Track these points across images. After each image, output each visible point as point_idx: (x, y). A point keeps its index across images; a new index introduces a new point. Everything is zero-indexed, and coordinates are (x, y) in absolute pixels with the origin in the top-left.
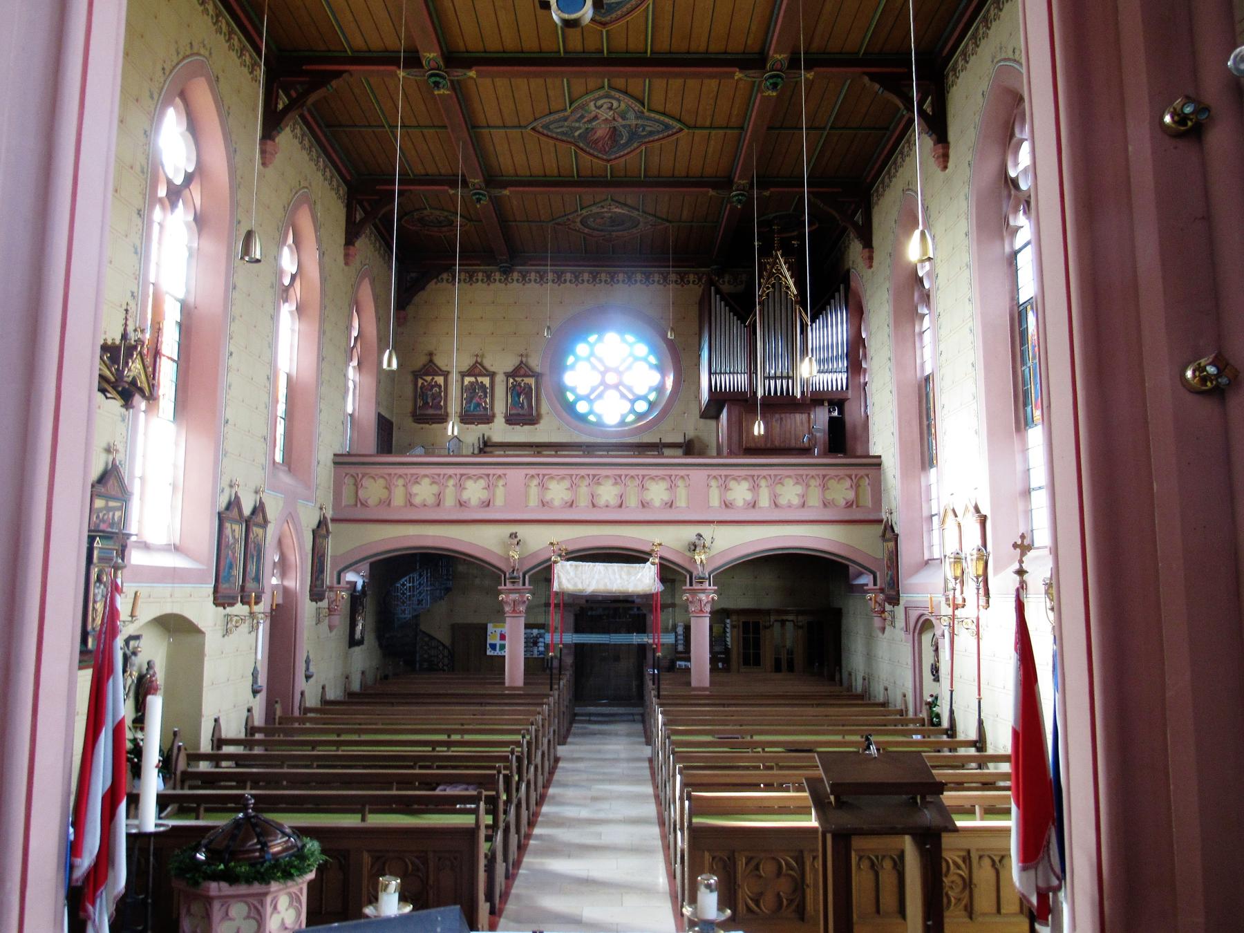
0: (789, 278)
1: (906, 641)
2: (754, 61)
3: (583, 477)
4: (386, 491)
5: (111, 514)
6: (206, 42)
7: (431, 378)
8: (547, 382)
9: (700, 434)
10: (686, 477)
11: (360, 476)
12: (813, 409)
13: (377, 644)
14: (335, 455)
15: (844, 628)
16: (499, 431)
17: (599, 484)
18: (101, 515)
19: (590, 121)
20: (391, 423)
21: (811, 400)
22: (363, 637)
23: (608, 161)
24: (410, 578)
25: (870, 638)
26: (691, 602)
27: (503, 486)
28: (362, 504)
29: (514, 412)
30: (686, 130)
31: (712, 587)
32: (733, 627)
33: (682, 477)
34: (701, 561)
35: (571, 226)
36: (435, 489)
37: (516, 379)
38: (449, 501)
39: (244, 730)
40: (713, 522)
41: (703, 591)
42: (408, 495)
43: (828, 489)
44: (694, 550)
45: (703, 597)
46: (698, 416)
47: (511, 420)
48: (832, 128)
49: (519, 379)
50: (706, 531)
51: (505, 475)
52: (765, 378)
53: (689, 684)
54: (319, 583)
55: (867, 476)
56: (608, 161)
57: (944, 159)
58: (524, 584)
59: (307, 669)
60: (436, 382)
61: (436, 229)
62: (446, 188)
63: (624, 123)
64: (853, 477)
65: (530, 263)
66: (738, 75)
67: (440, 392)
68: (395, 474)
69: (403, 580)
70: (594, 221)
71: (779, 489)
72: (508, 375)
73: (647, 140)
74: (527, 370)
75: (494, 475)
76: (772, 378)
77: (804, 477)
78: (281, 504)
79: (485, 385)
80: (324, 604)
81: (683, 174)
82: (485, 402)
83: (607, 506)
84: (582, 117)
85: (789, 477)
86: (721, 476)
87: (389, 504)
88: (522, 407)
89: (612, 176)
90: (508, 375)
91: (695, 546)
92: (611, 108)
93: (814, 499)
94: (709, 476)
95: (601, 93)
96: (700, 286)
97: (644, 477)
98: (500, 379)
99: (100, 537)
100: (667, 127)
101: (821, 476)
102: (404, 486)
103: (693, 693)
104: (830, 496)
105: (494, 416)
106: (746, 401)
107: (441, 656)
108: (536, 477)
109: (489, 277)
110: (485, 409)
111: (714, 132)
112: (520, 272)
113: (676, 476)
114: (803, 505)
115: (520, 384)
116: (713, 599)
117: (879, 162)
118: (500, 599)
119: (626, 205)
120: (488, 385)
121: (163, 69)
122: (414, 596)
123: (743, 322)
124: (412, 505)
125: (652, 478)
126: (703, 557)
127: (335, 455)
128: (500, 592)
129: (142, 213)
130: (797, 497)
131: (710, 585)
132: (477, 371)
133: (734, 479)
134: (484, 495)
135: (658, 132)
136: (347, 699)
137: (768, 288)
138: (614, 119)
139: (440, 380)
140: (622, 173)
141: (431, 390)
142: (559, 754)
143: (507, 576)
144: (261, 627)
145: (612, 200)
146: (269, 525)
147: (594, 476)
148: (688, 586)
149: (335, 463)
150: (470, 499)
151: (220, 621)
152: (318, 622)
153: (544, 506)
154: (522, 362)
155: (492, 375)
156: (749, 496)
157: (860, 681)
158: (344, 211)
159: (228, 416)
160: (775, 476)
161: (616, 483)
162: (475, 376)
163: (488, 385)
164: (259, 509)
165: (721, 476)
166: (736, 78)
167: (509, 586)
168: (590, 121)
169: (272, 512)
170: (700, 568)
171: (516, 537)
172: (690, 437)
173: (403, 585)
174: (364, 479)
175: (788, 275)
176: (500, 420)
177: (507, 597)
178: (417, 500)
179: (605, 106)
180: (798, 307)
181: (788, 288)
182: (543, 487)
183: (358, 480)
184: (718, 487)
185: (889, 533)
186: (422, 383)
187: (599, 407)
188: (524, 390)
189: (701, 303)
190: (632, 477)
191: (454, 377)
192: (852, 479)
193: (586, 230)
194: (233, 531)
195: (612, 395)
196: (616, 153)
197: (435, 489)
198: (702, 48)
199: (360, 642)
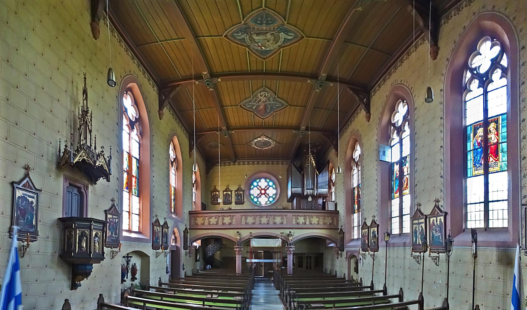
1: (346, 261)
2: (314, 76)
5: (114, 220)
6: (135, 72)
8: (247, 192)
14: (189, 211)
15: (324, 257)
16: (233, 206)
17: (262, 217)
18: (111, 220)
19: (258, 102)
20: (206, 205)
22: (199, 260)
23: (263, 119)
25: (333, 260)
29: (237, 201)
30: (288, 106)
32: (296, 258)
33: (285, 215)
38: (220, 223)
39: (168, 281)
40: (294, 228)
41: (291, 248)
47: (236, 203)
48: (332, 110)
49: (238, 192)
52: (306, 189)
54: (186, 245)
56: (263, 119)
57: (368, 118)
59: (183, 267)
61: (214, 149)
62: (216, 132)
63: (269, 103)
66: (309, 81)
71: (312, 219)
72: (235, 191)
73: (276, 110)
78: (173, 223)
80: (188, 251)
81: (286, 125)
84: (256, 100)
85: (315, 216)
88: (239, 200)
89: (264, 125)
90: (235, 191)
92: (265, 96)
93: (321, 222)
95: (262, 89)
99: (94, 221)
100: (283, 105)
103: (288, 276)
104: (325, 221)
105: (232, 202)
106: (301, 196)
109: (229, 164)
110: (230, 200)
111: (297, 107)
112: (238, 162)
114: (318, 224)
117: (353, 111)
120: (230, 194)
121: (121, 76)
123: (301, 173)
125: (277, 216)
126: (291, 238)
127: (189, 211)
129: (118, 124)
132: (227, 190)
133: (300, 216)
135: (280, 107)
138: (266, 101)
139: (218, 193)
140: (267, 125)
142: (253, 293)
144: (168, 255)
146: (169, 228)
147: (260, 215)
148: (287, 246)
151: (155, 254)
152: (186, 255)
155: (231, 191)
156: (304, 221)
157: (329, 271)
158: (189, 141)
159: (153, 195)
161: (266, 217)
163: (230, 194)
164: (166, 223)
166: (308, 82)
167: (237, 246)
168: (258, 102)
169: (170, 224)
170: (291, 241)
173: (210, 247)
176: (233, 203)
179: (263, 95)
181: (313, 164)
185: (342, 232)
189: (288, 170)
193: (256, 147)
194: (157, 229)
196: (266, 116)
197: (216, 220)
198: (297, 71)
199: (199, 261)
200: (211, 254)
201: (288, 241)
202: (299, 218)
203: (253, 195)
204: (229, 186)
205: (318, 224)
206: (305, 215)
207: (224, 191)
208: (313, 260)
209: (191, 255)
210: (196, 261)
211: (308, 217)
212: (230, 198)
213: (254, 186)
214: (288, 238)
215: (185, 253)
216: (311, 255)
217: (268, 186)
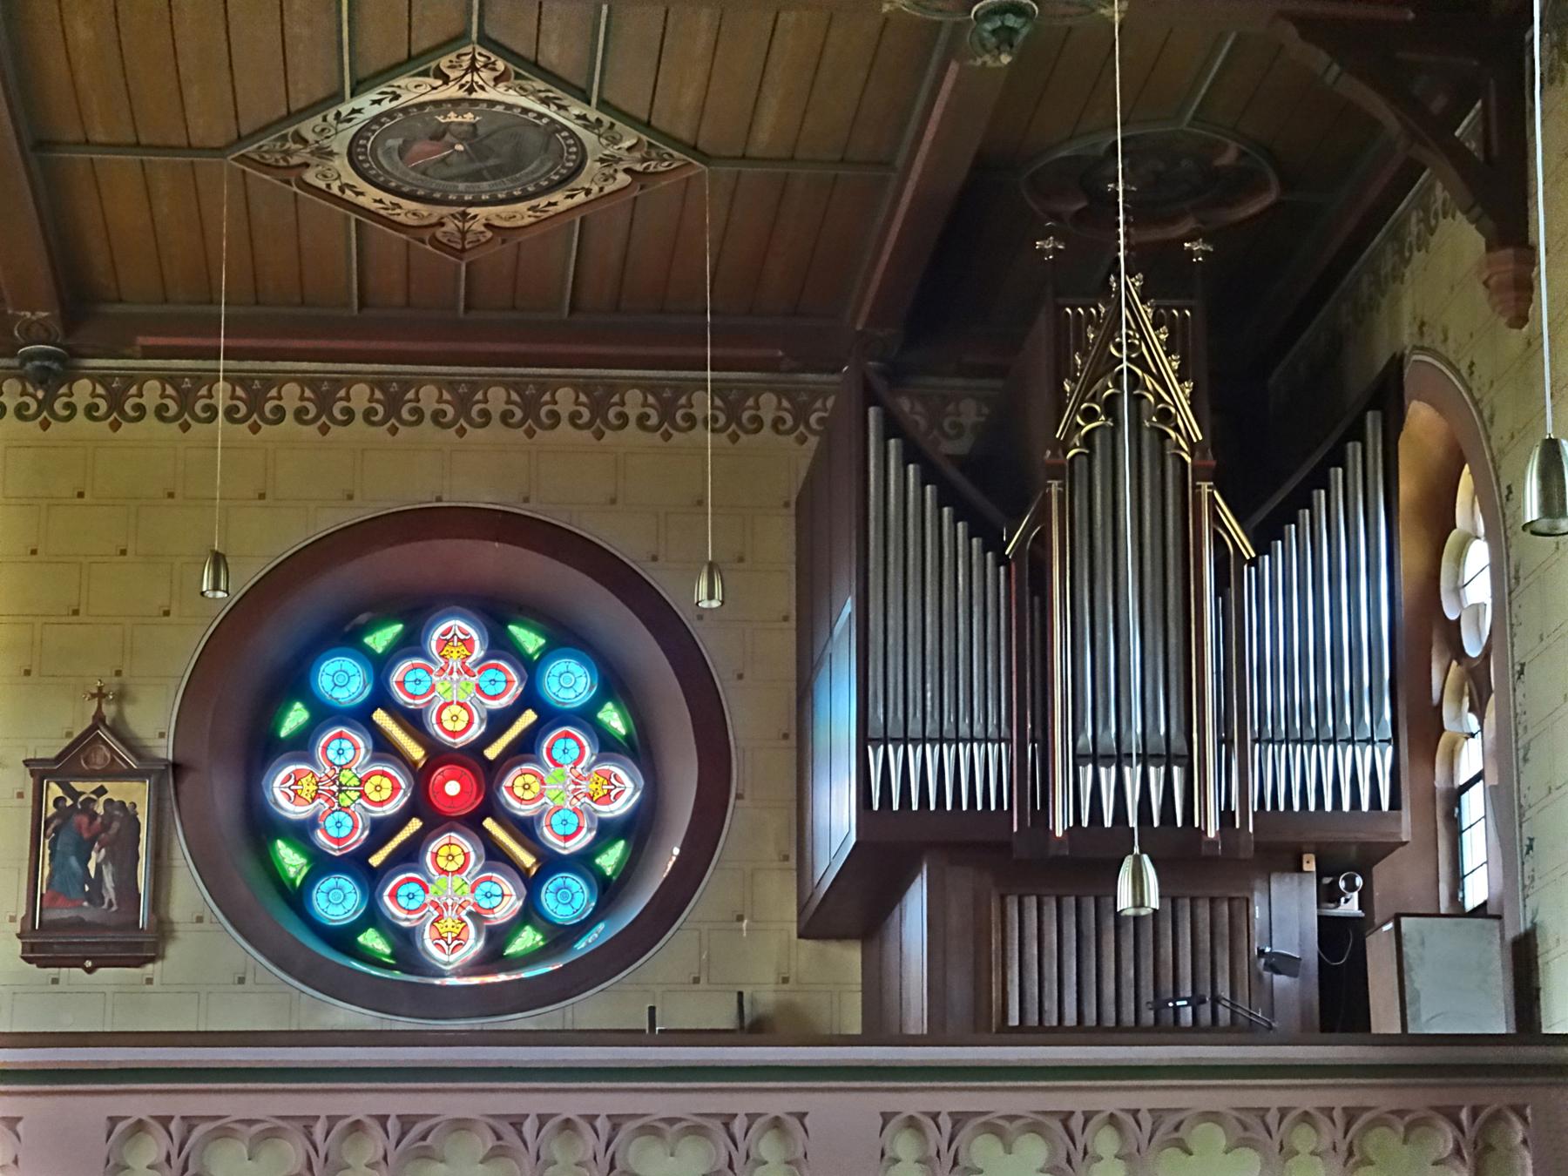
0: (1171, 378)
3: (357, 1126)
9: (798, 998)
10: (793, 1123)
12: (1259, 884)
21: (1258, 846)
35: (310, 176)
37: (78, 786)
46: (793, 929)
49: (85, 787)
52: (1079, 759)
55: (1519, 1111)
64: (1464, 1115)
65: (142, 340)
70: (402, 152)
76: (1107, 759)
77: (1272, 1118)
85: (1212, 1116)
86: (935, 1117)
88: (96, 896)
94: (886, 1117)
96: (802, 440)
97: (616, 1122)
101: (1337, 1114)
106: (1003, 847)
108: (157, 1128)
112: (101, 378)
113: (752, 1118)
119: (536, 68)
123: (994, 544)
125: (650, 1130)
137: (1090, 415)
145: (484, 40)
147: (407, 1122)
172: (761, 1010)
175: (1170, 366)
180: (1205, 487)
181: (1165, 416)
188: (106, 827)
190: (568, 1124)
192: (1458, 1125)
193: (370, 197)
203: (301, 833)
211: (1105, 1142)
213: (325, 715)
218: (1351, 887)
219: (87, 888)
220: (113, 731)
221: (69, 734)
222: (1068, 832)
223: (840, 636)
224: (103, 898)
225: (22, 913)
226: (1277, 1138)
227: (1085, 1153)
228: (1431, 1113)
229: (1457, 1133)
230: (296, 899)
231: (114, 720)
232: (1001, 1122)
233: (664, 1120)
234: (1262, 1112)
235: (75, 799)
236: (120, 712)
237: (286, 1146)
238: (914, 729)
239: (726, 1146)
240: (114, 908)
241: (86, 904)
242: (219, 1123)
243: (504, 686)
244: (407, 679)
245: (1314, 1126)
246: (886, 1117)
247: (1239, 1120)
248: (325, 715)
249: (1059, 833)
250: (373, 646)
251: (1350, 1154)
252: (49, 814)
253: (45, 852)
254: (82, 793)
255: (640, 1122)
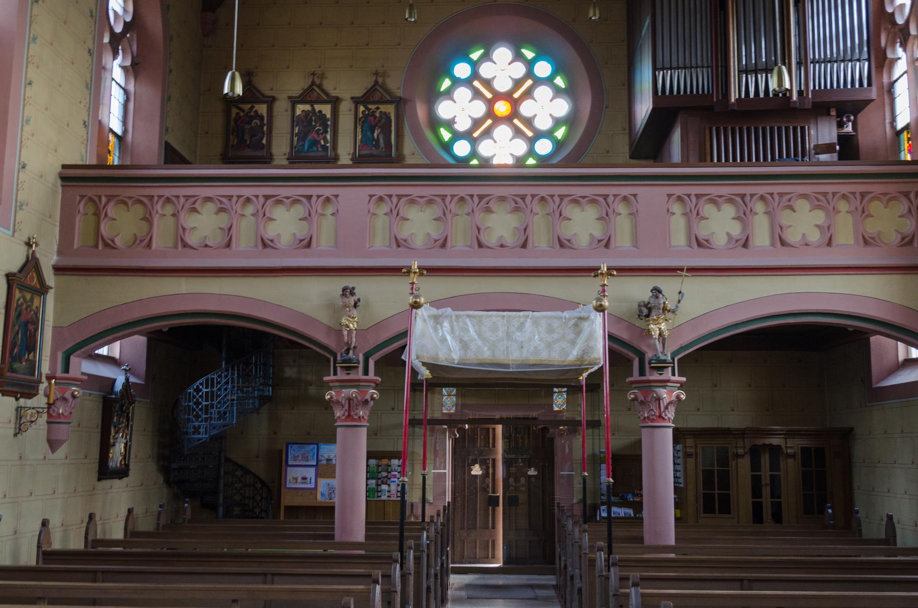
4: (144, 224)
7: (249, 106)
11: (104, 200)
13: (161, 479)
14: (64, 167)
17: (488, 210)
24: (207, 380)
26: (642, 403)
27: (332, 214)
28: (106, 245)
31: (677, 378)
33: (625, 199)
34: (660, 335)
36: (223, 220)
37: (370, 106)
41: (664, 383)
42: (181, 230)
43: (870, 216)
44: (648, 316)
45: (663, 393)
46: (628, 155)
50: (669, 286)
51: (336, 196)
53: (641, 540)
58: (366, 372)
60: (256, 112)
67: (262, 125)
68: (160, 197)
69: (198, 383)
71: (785, 217)
72: (357, 101)
74: (385, 94)
75: (319, 197)
77: (830, 196)
79: (325, 115)
82: (325, 139)
83: (502, 246)
85: (804, 196)
87: (149, 245)
88: (377, 146)
90: (357, 101)
91: (650, 310)
93: (845, 234)
98: (346, 108)
102: (173, 215)
104: (871, 227)
107: (258, 498)
110: (325, 148)
115: (373, 113)
116: (678, 397)
118: (327, 397)
120: (328, 116)
122: (212, 406)
124: (185, 245)
125: (575, 201)
128: (327, 386)
130: (817, 230)
131: (673, 374)
132: (314, 96)
133: (713, 201)
134: (301, 230)
136: (41, 565)
141: (250, 123)
143: (339, 358)
147: (481, 197)
148: (636, 376)
149: (64, 178)
150: (279, 235)
153: (399, 246)
154: (376, 82)
155: (335, 102)
156: (736, 229)
160: (781, 195)
161: (517, 209)
162: (311, 103)
163: (328, 116)
165: (689, 196)
167: (341, 375)
170: (659, 346)
171: (352, 294)
173: (198, 390)
174: (111, 204)
177: (338, 393)
178: (193, 239)
182: (395, 214)
183: (101, 207)
184: (684, 214)
186: (237, 114)
187: (485, 148)
188: (380, 121)
191: (281, 106)
195: (503, 132)
197: (223, 220)
199: (122, 473)
200: (203, 436)
201: (644, 348)
202: (708, 209)
203: (449, 124)
204: (323, 76)
205: (829, 244)
206: (743, 196)
207: (294, 101)
208: (790, 469)
209: (62, 431)
210: (105, 472)
211: (759, 207)
212: (328, 137)
213: (457, 82)
214: (639, 323)
215: (12, 415)
216: (775, 441)
217: (529, 82)
218: (849, 121)
219: (374, 143)
220: (381, 86)
221: (366, 88)
222: (736, 100)
223: (645, 35)
224: (379, 146)
225: (352, 151)
226: (832, 205)
227: (751, 211)
228: (898, 194)
229: (909, 203)
230: (447, 147)
231: (382, 83)
232: (716, 198)
233: (581, 197)
234: (825, 194)
235: (369, 111)
236: (384, 81)
237: (435, 207)
238: (674, 64)
239: (605, 207)
240: (384, 150)
241: (374, 148)
242: (410, 197)
243: (519, 70)
244: (486, 70)
245: (848, 201)
246: (669, 196)
247: (815, 197)
248: (457, 82)
249: (733, 100)
250: (473, 58)
251: (863, 212)
252: (361, 116)
253: (359, 130)
254: (371, 109)
255: (571, 198)
